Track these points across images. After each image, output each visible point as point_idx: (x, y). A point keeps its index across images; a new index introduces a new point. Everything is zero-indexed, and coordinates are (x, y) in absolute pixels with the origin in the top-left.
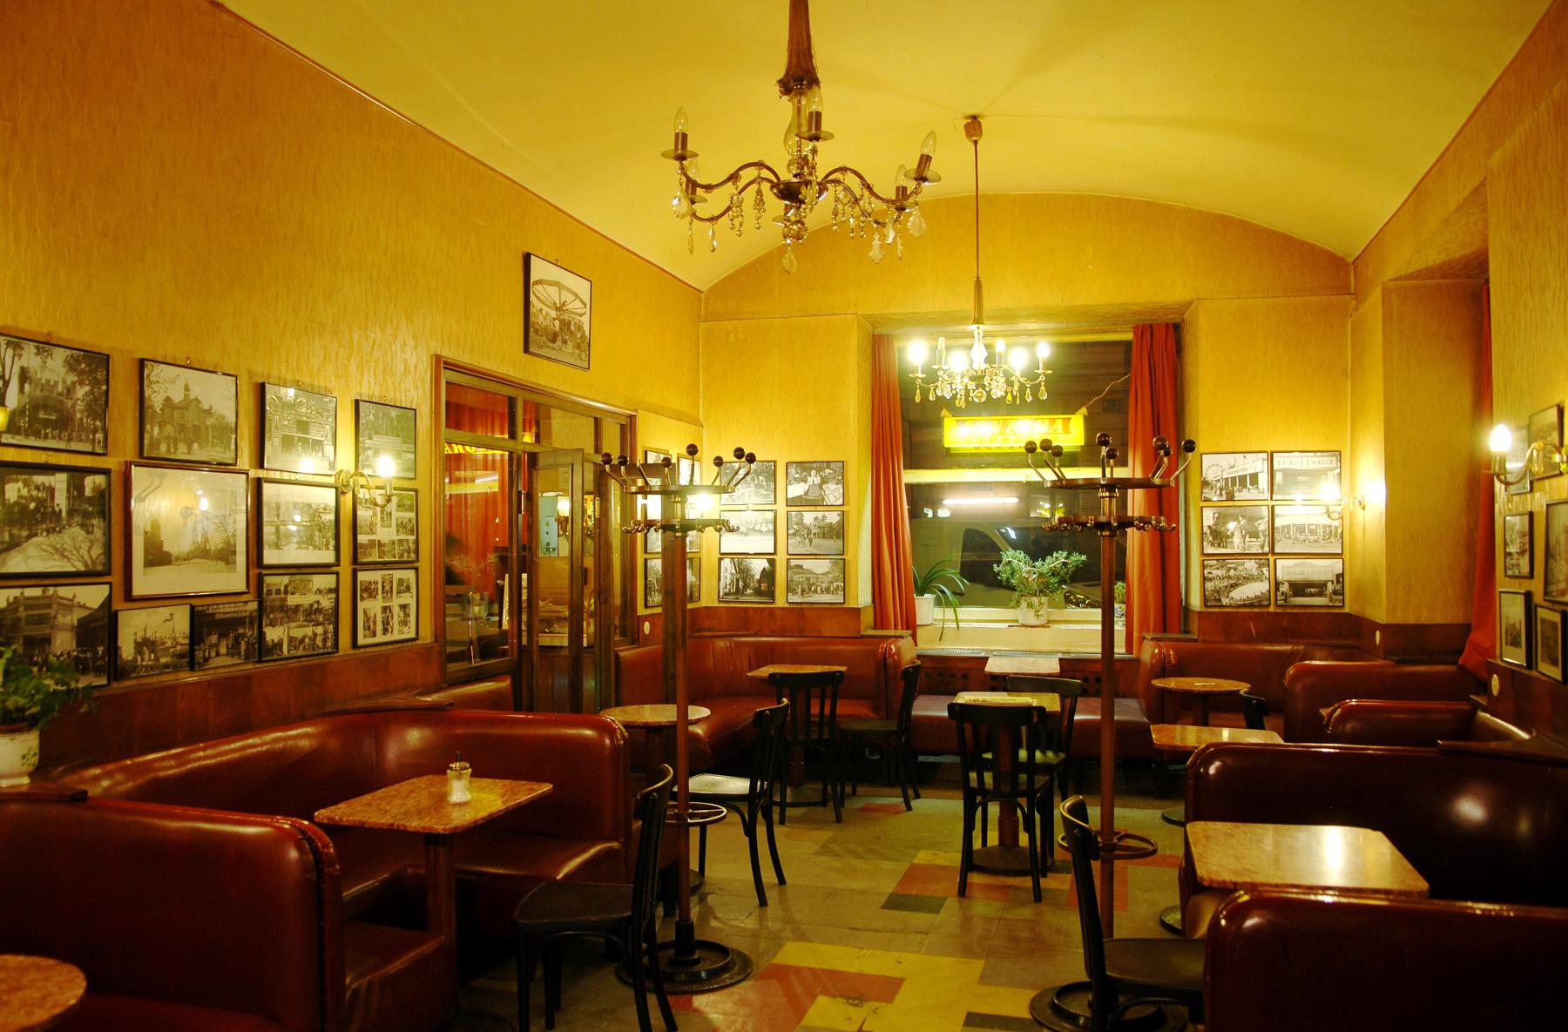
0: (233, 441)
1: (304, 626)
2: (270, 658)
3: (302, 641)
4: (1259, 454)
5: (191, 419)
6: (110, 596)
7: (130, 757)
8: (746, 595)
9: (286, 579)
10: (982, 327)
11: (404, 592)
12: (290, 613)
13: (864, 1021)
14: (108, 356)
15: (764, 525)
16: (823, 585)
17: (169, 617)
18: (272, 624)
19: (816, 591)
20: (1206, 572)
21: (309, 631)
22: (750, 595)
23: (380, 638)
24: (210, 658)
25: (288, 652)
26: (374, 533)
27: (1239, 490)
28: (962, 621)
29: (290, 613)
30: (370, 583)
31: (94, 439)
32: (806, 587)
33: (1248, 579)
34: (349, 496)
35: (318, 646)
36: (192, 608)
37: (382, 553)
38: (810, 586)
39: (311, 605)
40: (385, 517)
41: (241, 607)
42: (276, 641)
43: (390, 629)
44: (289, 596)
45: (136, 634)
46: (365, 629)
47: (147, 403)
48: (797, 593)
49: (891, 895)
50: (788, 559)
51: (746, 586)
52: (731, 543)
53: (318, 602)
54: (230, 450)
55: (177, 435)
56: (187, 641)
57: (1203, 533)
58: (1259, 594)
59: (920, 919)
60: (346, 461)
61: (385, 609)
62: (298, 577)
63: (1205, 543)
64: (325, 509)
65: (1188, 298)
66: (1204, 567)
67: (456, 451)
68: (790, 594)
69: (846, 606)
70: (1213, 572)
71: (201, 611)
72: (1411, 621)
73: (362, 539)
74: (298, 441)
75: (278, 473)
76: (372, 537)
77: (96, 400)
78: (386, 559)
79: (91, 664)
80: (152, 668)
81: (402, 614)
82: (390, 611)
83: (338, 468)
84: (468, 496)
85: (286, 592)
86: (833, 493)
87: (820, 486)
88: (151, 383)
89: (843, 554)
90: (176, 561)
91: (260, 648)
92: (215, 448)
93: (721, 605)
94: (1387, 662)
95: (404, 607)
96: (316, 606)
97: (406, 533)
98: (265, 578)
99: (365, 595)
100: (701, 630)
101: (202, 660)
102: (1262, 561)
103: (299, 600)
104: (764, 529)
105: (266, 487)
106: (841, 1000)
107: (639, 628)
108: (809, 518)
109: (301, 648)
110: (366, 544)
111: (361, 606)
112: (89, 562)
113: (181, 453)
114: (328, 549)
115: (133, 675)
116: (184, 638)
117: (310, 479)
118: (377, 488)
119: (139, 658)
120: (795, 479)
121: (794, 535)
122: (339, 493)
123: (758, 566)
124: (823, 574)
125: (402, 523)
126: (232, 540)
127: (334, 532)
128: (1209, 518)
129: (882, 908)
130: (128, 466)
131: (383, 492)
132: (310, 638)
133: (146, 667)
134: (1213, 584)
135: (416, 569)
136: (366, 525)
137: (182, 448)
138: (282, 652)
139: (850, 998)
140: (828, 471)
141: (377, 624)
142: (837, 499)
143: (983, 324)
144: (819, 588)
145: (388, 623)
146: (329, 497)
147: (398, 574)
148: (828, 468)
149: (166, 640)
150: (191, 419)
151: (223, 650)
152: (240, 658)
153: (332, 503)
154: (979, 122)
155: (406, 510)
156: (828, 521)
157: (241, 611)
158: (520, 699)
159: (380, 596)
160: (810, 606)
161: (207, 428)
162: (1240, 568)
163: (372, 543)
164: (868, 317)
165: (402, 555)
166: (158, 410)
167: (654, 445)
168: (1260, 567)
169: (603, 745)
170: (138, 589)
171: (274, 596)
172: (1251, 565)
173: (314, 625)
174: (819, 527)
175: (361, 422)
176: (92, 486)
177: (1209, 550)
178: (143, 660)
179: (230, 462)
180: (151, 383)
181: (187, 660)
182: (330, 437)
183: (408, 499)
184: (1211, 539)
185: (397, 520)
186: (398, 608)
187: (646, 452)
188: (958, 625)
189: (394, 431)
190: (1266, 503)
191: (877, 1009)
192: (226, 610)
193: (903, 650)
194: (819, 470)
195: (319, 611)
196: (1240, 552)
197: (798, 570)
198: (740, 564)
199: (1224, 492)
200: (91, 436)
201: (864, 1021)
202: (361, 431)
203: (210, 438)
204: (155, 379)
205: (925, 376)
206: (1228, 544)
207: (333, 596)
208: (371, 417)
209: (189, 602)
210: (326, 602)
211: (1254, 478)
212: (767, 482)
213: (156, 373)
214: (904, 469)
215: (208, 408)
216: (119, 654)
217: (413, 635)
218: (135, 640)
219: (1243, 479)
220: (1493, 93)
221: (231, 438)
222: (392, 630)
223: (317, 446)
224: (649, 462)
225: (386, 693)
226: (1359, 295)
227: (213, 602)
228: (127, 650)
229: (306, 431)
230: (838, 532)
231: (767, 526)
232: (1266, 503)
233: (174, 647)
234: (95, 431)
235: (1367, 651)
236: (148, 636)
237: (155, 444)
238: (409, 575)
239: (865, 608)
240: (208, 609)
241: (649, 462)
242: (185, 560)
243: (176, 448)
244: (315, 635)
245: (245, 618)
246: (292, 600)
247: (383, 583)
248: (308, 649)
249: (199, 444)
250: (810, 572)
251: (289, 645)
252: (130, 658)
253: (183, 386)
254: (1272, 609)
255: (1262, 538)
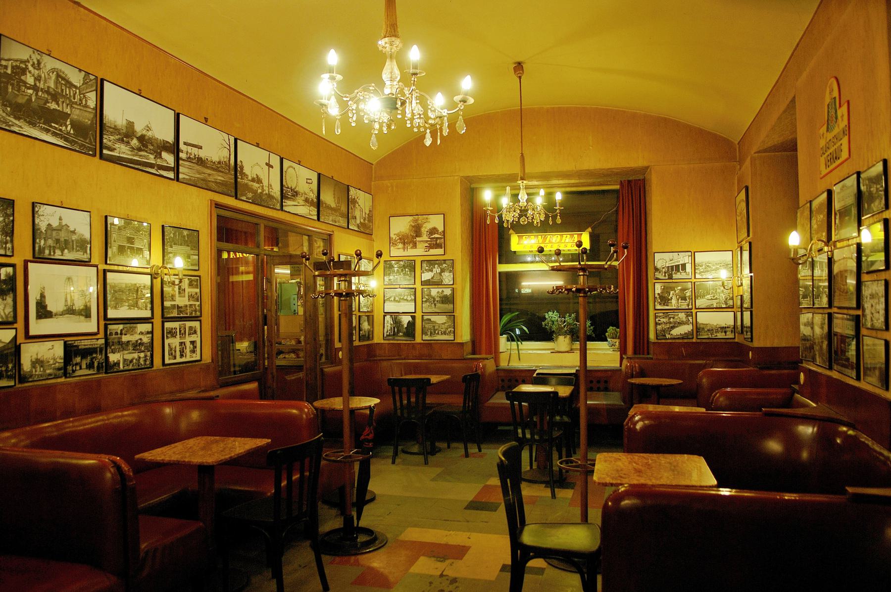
0: (88, 249)
1: (133, 353)
2: (112, 371)
3: (131, 361)
4: (686, 253)
5: (63, 236)
6: (16, 337)
7: (29, 425)
8: (399, 336)
9: (121, 327)
10: (525, 182)
11: (193, 334)
12: (124, 346)
13: (445, 569)
14: (14, 201)
15: (409, 296)
16: (442, 330)
17: (51, 348)
18: (113, 352)
19: (438, 334)
20: (657, 320)
21: (136, 355)
22: (401, 336)
23: (179, 360)
24: (76, 370)
25: (124, 367)
26: (175, 301)
27: (675, 273)
28: (522, 350)
29: (124, 345)
30: (172, 329)
31: (6, 247)
32: (433, 331)
33: (681, 323)
34: (159, 279)
35: (141, 364)
36: (65, 343)
37: (180, 312)
38: (435, 330)
39: (137, 341)
40: (181, 291)
41: (94, 342)
42: (115, 361)
43: (184, 355)
44: (123, 336)
45: (31, 357)
46: (169, 354)
47: (37, 227)
48: (427, 335)
49: (471, 501)
50: (422, 316)
51: (399, 331)
52: (390, 307)
53: (141, 339)
54: (87, 254)
55: (54, 245)
56: (62, 361)
57: (655, 298)
58: (687, 332)
59: (484, 514)
60: (156, 259)
61: (181, 344)
62: (128, 325)
63: (656, 303)
64: (144, 287)
65: (645, 164)
66: (656, 317)
67: (238, 256)
68: (424, 335)
69: (455, 341)
70: (661, 320)
71: (70, 344)
72: (768, 345)
73: (167, 304)
74: (128, 249)
75: (116, 267)
76: (173, 303)
77: (7, 225)
78: (182, 315)
79: (5, 374)
80: (41, 375)
81: (192, 346)
82: (184, 345)
83: (152, 263)
84: (244, 282)
85: (121, 334)
86: (447, 278)
87: (440, 274)
88: (39, 216)
89: (453, 313)
90: (55, 316)
91: (106, 365)
92: (78, 252)
93: (385, 342)
94: (756, 369)
95: (193, 343)
96: (139, 341)
97: (194, 301)
98: (109, 326)
99: (169, 336)
100: (375, 356)
101: (71, 372)
102: (688, 313)
103: (130, 338)
104: (409, 298)
105: (109, 275)
106: (433, 559)
107: (336, 355)
108: (434, 292)
109: (131, 365)
110: (169, 307)
111: (167, 342)
112: (4, 316)
113: (58, 255)
114: (146, 309)
115: (30, 380)
116: (61, 359)
117: (135, 270)
118: (174, 275)
119: (34, 370)
120: (426, 270)
121: (426, 301)
122: (153, 276)
123: (405, 320)
124: (442, 324)
125: (191, 295)
126: (88, 304)
127: (150, 300)
128: (658, 289)
129: (465, 509)
130: (26, 262)
131: (177, 277)
132: (136, 360)
133: (38, 375)
134: (661, 327)
135: (200, 321)
136: (170, 296)
137: (58, 252)
138: (119, 367)
139: (437, 558)
140: (444, 265)
141: (177, 352)
142: (450, 281)
143: (525, 180)
144: (440, 332)
145: (183, 352)
146: (147, 280)
147: (189, 324)
148: (445, 263)
149: (50, 360)
150: (63, 236)
151: (84, 366)
152: (94, 371)
153: (149, 283)
154: (522, 66)
155: (193, 288)
156: (445, 293)
157: (95, 344)
158: (263, 393)
159: (178, 336)
160: (435, 342)
161: (73, 241)
162: (676, 317)
163: (173, 306)
164: (467, 178)
165: (192, 313)
166: (43, 231)
167: (344, 252)
168: (687, 317)
169: (302, 418)
170: (32, 332)
171: (114, 336)
172: (682, 316)
173: (138, 352)
174: (440, 297)
175: (165, 238)
176: (5, 273)
177: (658, 307)
178: (36, 371)
179: (87, 260)
180: (39, 216)
181: (62, 371)
182: (147, 246)
183: (195, 282)
184: (659, 301)
185: (189, 293)
186: (189, 343)
187: (339, 255)
188: (519, 352)
189: (185, 243)
190: (690, 280)
191: (453, 563)
192: (85, 343)
193: (487, 367)
194: (439, 265)
195: (142, 344)
196: (675, 308)
197: (428, 322)
198: (396, 318)
199: (666, 274)
200: (4, 246)
201: (445, 569)
202: (166, 243)
203: (75, 247)
204: (42, 214)
205: (492, 208)
206: (669, 304)
207: (150, 335)
208: (172, 235)
209: (63, 339)
210: (146, 339)
211: (684, 266)
212: (410, 272)
213: (43, 210)
214: (499, 263)
215: (73, 230)
216: (21, 368)
217: (198, 358)
218: (31, 360)
219: (677, 266)
220: (800, 45)
221: (87, 247)
222: (186, 355)
223: (140, 250)
224: (341, 260)
225: (183, 391)
226: (741, 162)
227: (78, 339)
228: (26, 365)
229: (132, 243)
230: (449, 300)
231: (411, 297)
232: (690, 280)
233: (55, 364)
234: (6, 243)
235: (745, 362)
236: (39, 358)
237: (42, 250)
238: (196, 324)
239: (466, 343)
240: (75, 343)
241: (341, 260)
242: (61, 315)
243: (54, 252)
244: (139, 358)
245: (97, 348)
246: (125, 338)
247: (180, 329)
248: (135, 365)
249: (68, 250)
250: (435, 322)
251: (124, 363)
252: (29, 370)
253: (58, 218)
254: (694, 340)
255: (688, 300)
